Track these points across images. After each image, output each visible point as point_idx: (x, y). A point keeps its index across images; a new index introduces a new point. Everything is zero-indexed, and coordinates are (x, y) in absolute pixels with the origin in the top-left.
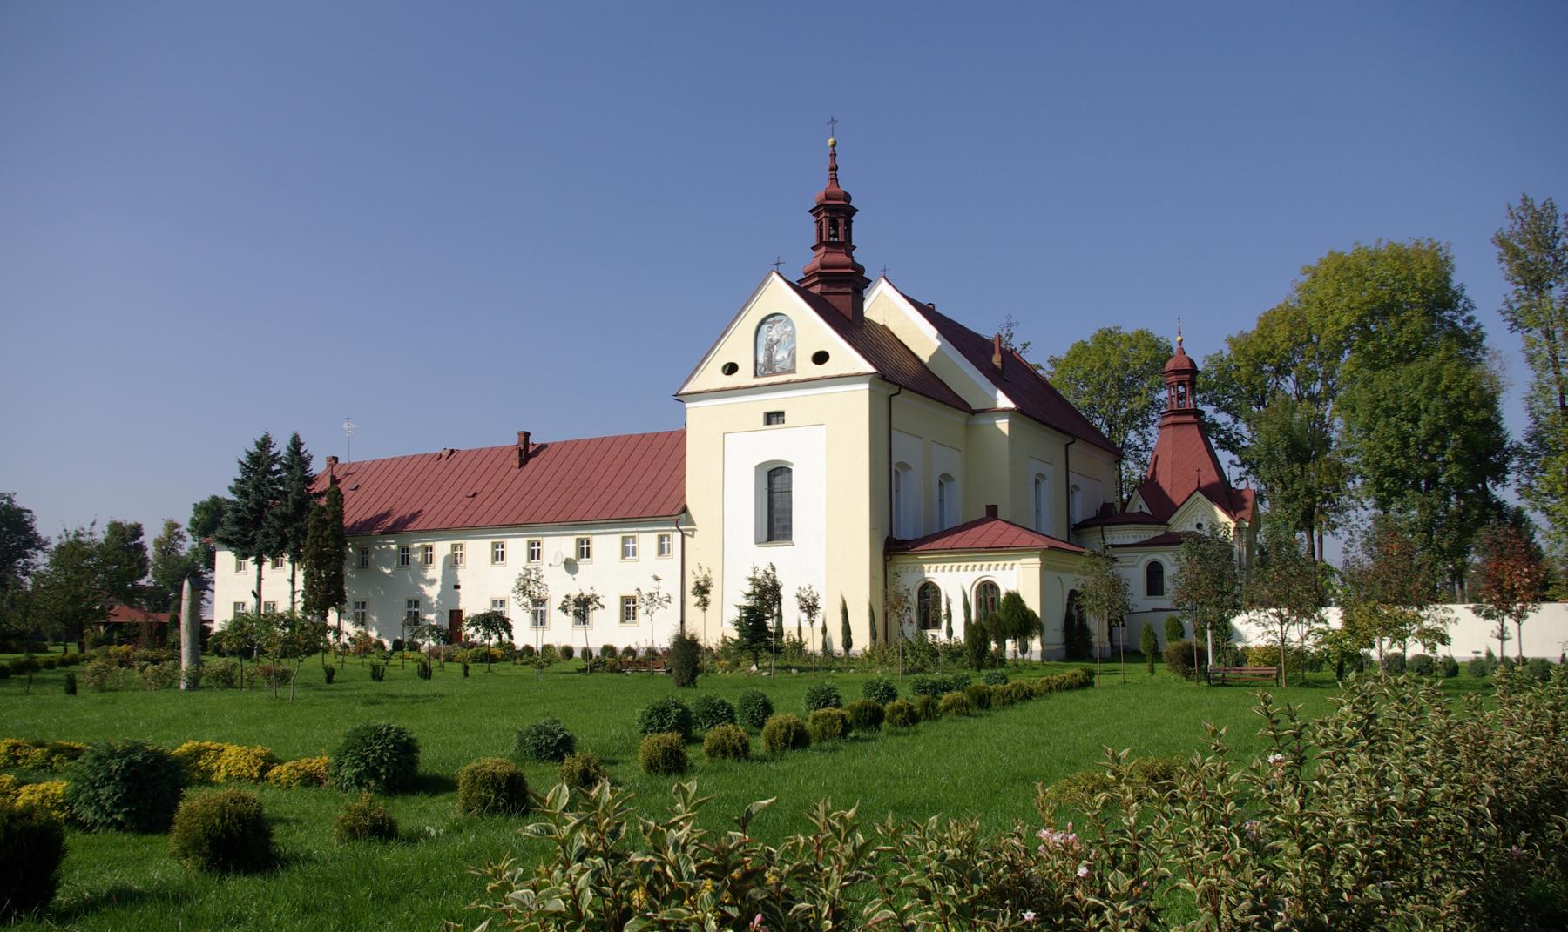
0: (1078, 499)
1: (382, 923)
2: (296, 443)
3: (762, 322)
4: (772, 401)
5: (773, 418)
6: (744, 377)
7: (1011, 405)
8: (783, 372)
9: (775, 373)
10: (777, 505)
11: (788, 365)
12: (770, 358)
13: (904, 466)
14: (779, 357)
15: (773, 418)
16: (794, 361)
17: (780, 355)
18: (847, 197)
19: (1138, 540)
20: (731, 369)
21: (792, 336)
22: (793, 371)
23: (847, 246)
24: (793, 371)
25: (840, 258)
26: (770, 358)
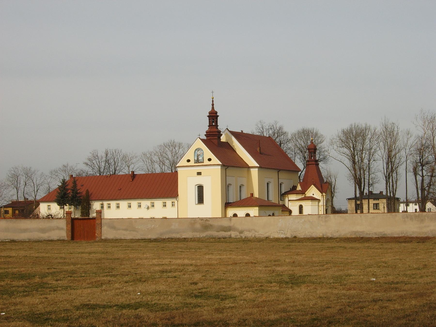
0: (283, 186)
1: (85, 272)
2: (87, 192)
3: (196, 150)
4: (199, 169)
5: (199, 174)
6: (192, 163)
7: (259, 166)
8: (201, 162)
9: (199, 163)
10: (172, 245)
11: (202, 161)
12: (198, 159)
13: (230, 184)
14: (200, 159)
15: (199, 174)
16: (203, 160)
17: (200, 158)
18: (216, 113)
19: (297, 199)
20: (189, 161)
21: (203, 154)
22: (203, 162)
23: (217, 126)
24: (203, 162)
25: (215, 130)
26: (198, 159)
